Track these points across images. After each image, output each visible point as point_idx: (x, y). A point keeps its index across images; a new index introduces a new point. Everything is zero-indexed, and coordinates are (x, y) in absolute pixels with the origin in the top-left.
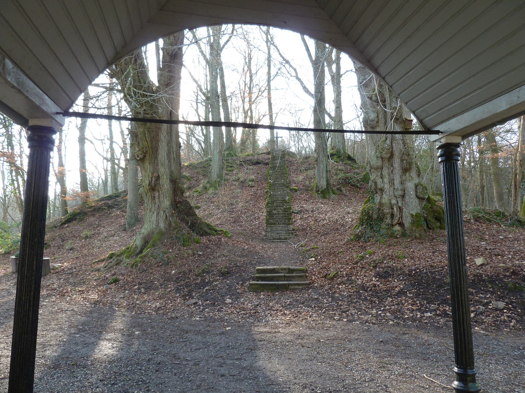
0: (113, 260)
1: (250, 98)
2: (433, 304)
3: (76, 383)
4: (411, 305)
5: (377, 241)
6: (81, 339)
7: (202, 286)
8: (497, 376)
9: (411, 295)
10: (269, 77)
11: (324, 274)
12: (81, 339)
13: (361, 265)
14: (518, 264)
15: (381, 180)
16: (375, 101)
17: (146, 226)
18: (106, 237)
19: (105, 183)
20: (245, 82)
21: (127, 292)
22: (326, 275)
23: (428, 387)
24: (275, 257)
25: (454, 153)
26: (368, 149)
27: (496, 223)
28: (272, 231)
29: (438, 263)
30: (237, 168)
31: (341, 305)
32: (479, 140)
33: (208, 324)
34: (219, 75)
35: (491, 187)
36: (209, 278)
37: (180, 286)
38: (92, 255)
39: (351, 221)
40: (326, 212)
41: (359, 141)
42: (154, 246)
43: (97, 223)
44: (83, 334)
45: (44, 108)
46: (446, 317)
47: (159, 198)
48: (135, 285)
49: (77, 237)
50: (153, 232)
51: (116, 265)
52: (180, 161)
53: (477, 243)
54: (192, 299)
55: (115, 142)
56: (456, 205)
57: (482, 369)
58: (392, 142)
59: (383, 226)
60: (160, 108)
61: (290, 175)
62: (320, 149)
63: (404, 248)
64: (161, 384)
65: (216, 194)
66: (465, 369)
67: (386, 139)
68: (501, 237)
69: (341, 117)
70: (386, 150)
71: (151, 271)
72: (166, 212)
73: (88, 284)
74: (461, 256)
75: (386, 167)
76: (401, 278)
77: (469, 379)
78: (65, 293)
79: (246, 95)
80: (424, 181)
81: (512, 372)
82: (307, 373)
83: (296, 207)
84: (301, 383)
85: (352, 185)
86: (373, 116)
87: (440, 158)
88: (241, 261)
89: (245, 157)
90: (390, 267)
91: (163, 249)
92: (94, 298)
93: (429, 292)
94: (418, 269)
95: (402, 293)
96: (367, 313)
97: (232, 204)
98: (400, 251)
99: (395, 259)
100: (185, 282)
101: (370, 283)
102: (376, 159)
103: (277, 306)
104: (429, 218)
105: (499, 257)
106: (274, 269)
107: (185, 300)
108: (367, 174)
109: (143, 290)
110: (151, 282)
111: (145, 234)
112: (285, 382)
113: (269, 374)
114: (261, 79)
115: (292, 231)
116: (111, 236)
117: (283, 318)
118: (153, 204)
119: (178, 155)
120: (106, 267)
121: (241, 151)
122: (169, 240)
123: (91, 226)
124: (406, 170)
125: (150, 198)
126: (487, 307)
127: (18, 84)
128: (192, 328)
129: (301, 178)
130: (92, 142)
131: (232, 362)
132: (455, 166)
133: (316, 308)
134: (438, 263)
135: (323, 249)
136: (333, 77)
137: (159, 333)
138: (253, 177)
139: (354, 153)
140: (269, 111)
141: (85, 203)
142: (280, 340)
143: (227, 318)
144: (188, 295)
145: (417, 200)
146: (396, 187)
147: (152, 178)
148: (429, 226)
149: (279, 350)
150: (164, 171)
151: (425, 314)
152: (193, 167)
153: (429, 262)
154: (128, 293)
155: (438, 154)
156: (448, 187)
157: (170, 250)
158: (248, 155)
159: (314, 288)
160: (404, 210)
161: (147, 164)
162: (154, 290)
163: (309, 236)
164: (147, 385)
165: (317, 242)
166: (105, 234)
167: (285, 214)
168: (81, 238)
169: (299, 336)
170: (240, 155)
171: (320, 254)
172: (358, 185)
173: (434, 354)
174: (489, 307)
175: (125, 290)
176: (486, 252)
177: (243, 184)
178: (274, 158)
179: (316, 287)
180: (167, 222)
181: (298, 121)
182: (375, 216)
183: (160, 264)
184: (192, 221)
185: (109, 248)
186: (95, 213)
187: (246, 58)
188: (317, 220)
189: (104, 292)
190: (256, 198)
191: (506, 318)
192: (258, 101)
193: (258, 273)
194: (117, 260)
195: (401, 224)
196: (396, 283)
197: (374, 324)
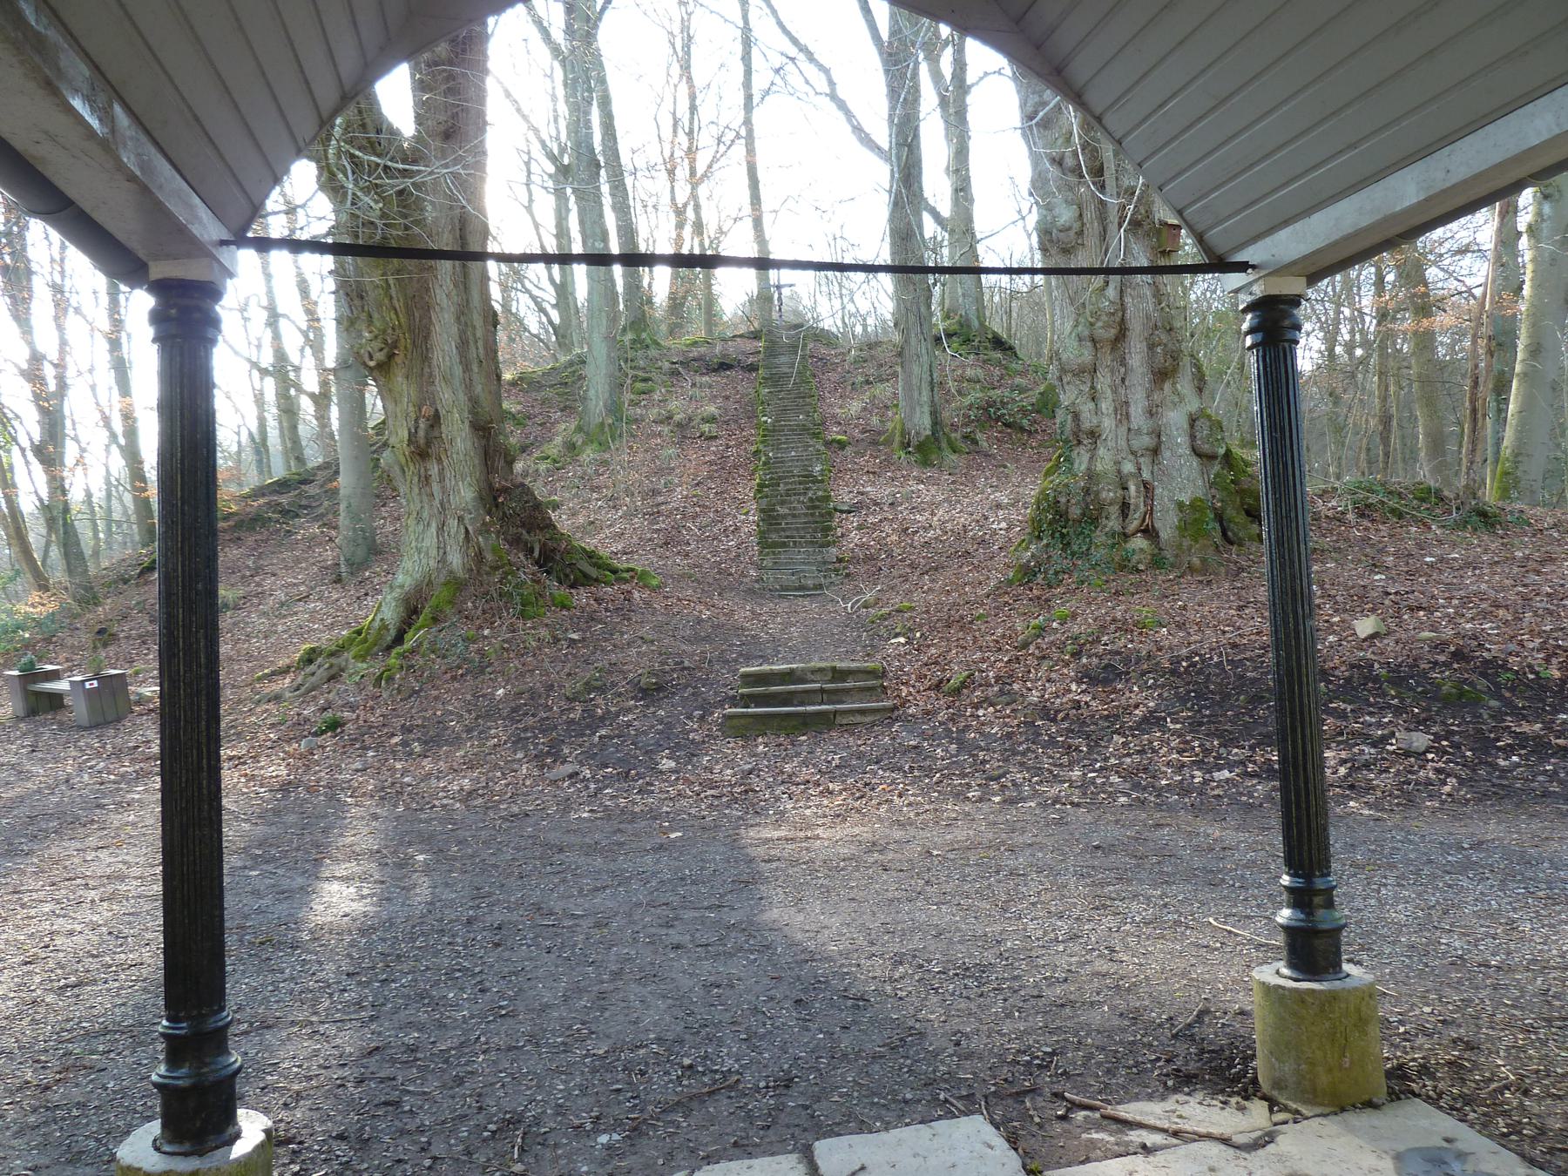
0: (319, 667)
1: (693, 172)
4: (1178, 753)
5: (1083, 582)
6: (267, 881)
7: (588, 726)
8: (1398, 914)
9: (1178, 726)
10: (749, 98)
12: (267, 881)
13: (1037, 652)
14: (1471, 629)
15: (1091, 405)
16: (1073, 171)
17: (407, 564)
18: (282, 604)
20: (674, 114)
21: (371, 754)
22: (941, 681)
23: (1218, 945)
24: (790, 639)
25: (1287, 323)
26: (1053, 316)
27: (1416, 521)
28: (776, 566)
29: (1253, 637)
30: (664, 382)
31: (984, 762)
32: (1380, 282)
33: (616, 826)
34: (603, 172)
35: (1413, 419)
36: (607, 704)
37: (525, 730)
39: (1006, 530)
40: (933, 506)
41: (1025, 289)
42: (435, 620)
43: (250, 563)
44: (270, 867)
45: (195, 230)
46: (1272, 780)
47: (442, 480)
48: (393, 735)
50: (430, 583)
52: (497, 368)
53: (1361, 577)
54: (562, 763)
55: (284, 316)
56: (1290, 462)
57: (1359, 899)
58: (1122, 291)
59: (1099, 537)
60: (429, 208)
61: (821, 398)
62: (912, 318)
63: (1158, 599)
64: (514, 973)
65: (605, 463)
66: (1308, 877)
67: (1107, 283)
68: (1428, 559)
69: (969, 220)
70: (1104, 318)
71: (435, 693)
72: (467, 521)
73: (252, 739)
74: (1302, 593)
76: (1151, 681)
77: (1317, 900)
80: (1218, 406)
81: (1438, 902)
82: (903, 930)
83: (844, 495)
85: (1007, 425)
86: (1066, 215)
90: (1118, 653)
91: (465, 630)
94: (1197, 654)
95: (1152, 721)
96: (1056, 779)
97: (655, 492)
98: (1146, 609)
99: (1132, 631)
101: (1065, 700)
102: (1076, 344)
103: (806, 774)
104: (1230, 512)
105: (1422, 613)
106: (792, 671)
107: (542, 767)
108: (1052, 388)
109: (417, 747)
110: (439, 722)
112: (846, 954)
113: (799, 936)
114: (722, 108)
117: (826, 802)
118: (425, 498)
121: (671, 332)
122: (481, 603)
123: (233, 573)
124: (1162, 375)
125: (416, 479)
126: (1383, 748)
127: (142, 169)
128: (573, 839)
129: (855, 407)
131: (697, 915)
132: (1289, 358)
133: (916, 773)
134: (1253, 637)
135: (927, 612)
136: (944, 103)
137: (484, 856)
138: (712, 409)
139: (1009, 329)
140: (752, 204)
144: (548, 753)
145: (1195, 462)
146: (1134, 426)
147: (416, 421)
148: (1230, 534)
149: (820, 881)
150: (451, 400)
151: (1216, 775)
152: (529, 384)
153: (1228, 635)
155: (1245, 326)
156: (1269, 415)
157: (486, 632)
158: (695, 344)
159: (908, 720)
160: (1158, 491)
161: (400, 379)
162: (451, 744)
163: (886, 577)
164: (478, 979)
167: (812, 515)
169: (874, 844)
171: (921, 626)
172: (1025, 422)
174: (1388, 747)
175: (365, 748)
176: (1387, 602)
178: (772, 351)
182: (1075, 512)
183: (460, 672)
184: (544, 545)
185: (296, 634)
186: (242, 535)
188: (907, 529)
189: (302, 756)
190: (723, 470)
191: (1431, 775)
193: (746, 684)
194: (331, 666)
195: (1149, 532)
196: (1135, 694)
197: (1078, 805)
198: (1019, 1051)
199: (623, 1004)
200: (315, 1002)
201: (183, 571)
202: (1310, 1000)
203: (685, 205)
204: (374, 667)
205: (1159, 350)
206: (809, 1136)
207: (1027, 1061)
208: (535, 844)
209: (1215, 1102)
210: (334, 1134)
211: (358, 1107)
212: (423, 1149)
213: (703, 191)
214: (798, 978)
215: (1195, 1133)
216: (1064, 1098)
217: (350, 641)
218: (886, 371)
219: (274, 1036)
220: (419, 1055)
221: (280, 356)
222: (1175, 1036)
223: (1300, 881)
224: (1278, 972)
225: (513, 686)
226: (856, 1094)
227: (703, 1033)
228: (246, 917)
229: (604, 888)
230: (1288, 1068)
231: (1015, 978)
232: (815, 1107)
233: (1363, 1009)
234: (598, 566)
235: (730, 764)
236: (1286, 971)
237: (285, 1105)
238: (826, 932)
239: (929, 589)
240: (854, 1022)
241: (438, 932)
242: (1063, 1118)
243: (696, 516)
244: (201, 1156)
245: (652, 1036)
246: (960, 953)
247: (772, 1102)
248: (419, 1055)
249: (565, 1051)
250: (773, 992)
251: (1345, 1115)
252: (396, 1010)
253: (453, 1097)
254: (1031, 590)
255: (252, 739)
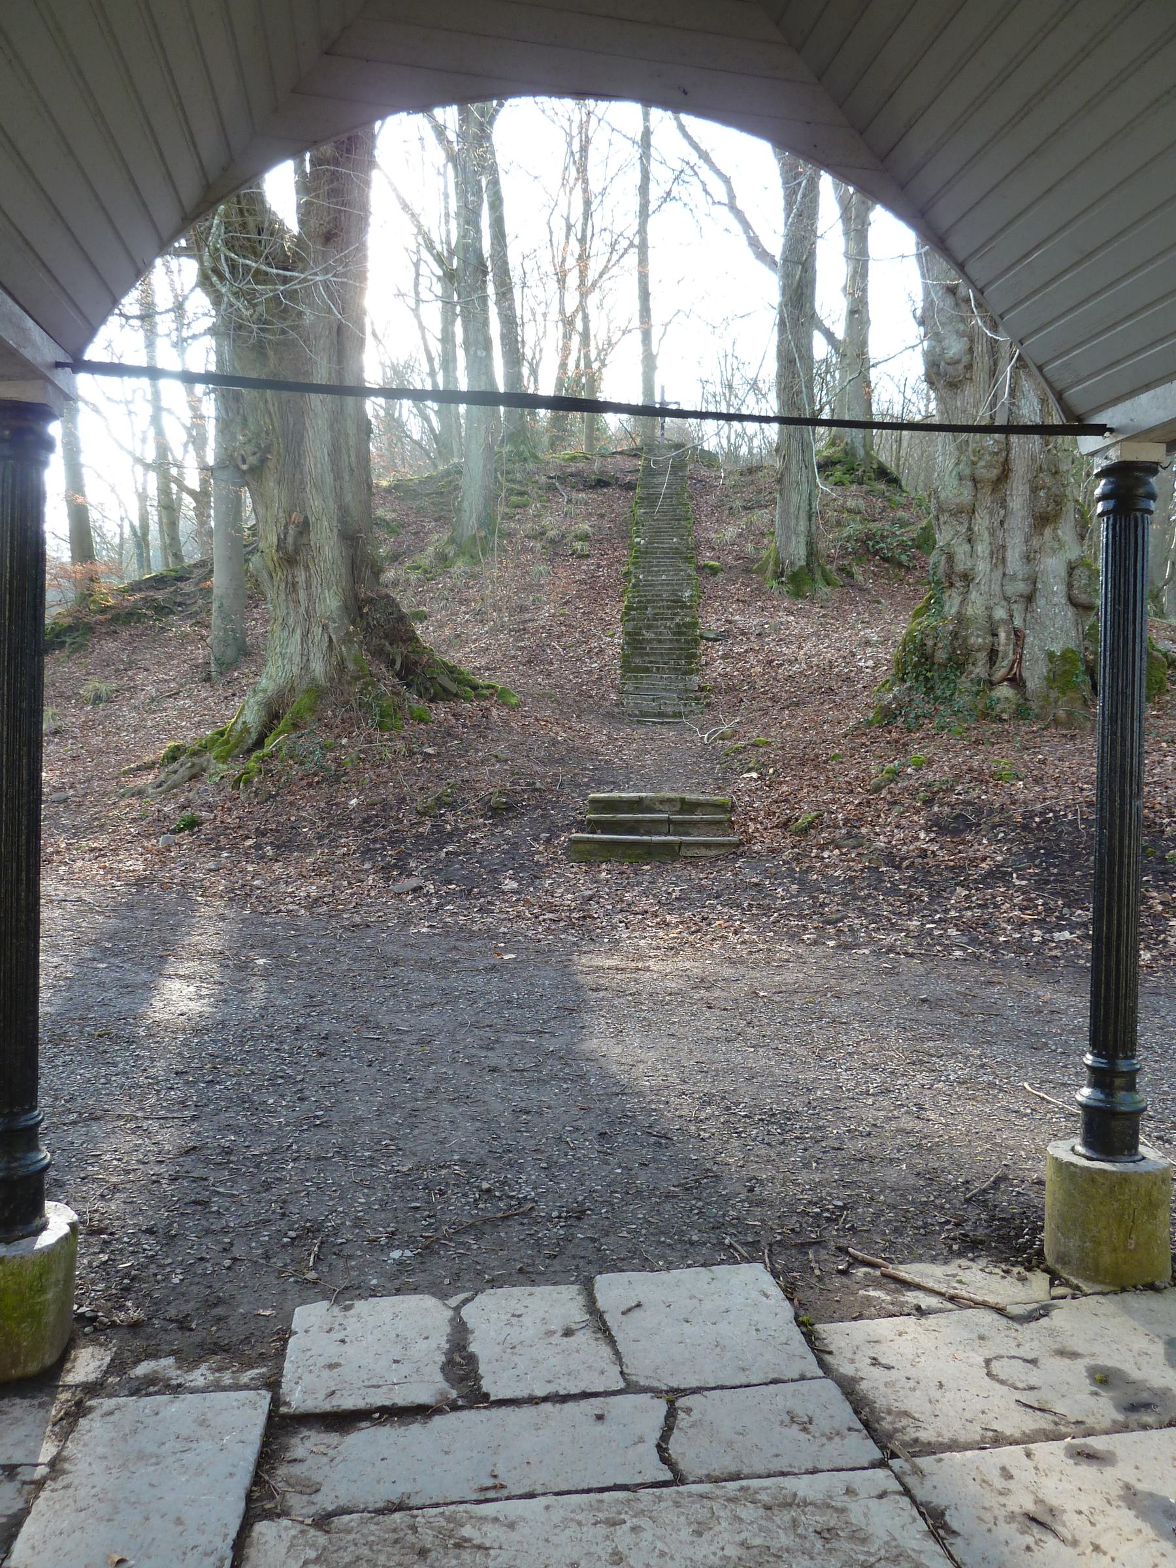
2: (1081, 909)
3: (114, 1078)
4: (1020, 910)
5: (943, 728)
7: (436, 841)
9: (1024, 883)
11: (783, 818)
12: (113, 974)
13: (889, 796)
15: (967, 547)
17: (270, 669)
18: (153, 700)
19: (141, 539)
20: (567, 219)
21: (225, 854)
22: (789, 820)
23: (1029, 1111)
24: (644, 766)
25: (1141, 491)
28: (637, 691)
31: (823, 905)
33: (452, 944)
34: (490, 277)
36: (456, 821)
37: (375, 841)
38: (118, 751)
40: (802, 639)
42: (295, 726)
43: (125, 657)
44: (116, 961)
45: (28, 353)
47: (308, 587)
48: (247, 837)
49: (69, 698)
50: (292, 689)
51: (190, 779)
52: (369, 476)
55: (168, 410)
56: (1131, 636)
59: (964, 683)
61: (697, 522)
62: (794, 444)
63: (1019, 751)
64: (335, 1085)
65: (473, 576)
69: (864, 344)
72: (331, 630)
73: (114, 832)
75: (986, 508)
77: (1118, 1082)
78: (52, 854)
79: (571, 262)
82: (717, 1070)
83: (711, 623)
84: (698, 1092)
85: (885, 559)
87: (1100, 503)
88: (545, 776)
89: (563, 463)
90: (970, 803)
91: (324, 738)
92: (134, 871)
93: (1073, 875)
94: (1051, 811)
95: (997, 875)
97: (523, 609)
99: (987, 782)
100: (387, 831)
101: (911, 848)
102: (956, 482)
103: (645, 903)
106: (641, 800)
107: (388, 879)
109: (269, 851)
110: (292, 828)
111: (269, 694)
113: (614, 1068)
115: (698, 694)
116: (170, 696)
117: (661, 934)
118: (291, 605)
119: (364, 459)
120: (160, 786)
121: (552, 445)
122: (340, 712)
123: (108, 665)
124: (1043, 520)
128: (409, 953)
130: (96, 409)
131: (518, 1039)
132: (1140, 529)
135: (783, 748)
137: (322, 965)
138: (586, 527)
140: (642, 316)
141: (86, 596)
142: (649, 989)
143: (506, 930)
144: (395, 865)
145: (1070, 612)
146: (1010, 571)
147: (286, 527)
149: (643, 1014)
151: (1056, 935)
153: (1086, 793)
154: (227, 857)
155: (1098, 492)
156: (1114, 587)
157: (344, 741)
158: (573, 459)
159: (752, 856)
160: (1029, 640)
161: (272, 484)
162: (302, 850)
163: (746, 708)
164: (299, 1087)
165: (769, 726)
166: (152, 690)
167: (677, 641)
168: (82, 702)
169: (702, 981)
170: (547, 456)
171: (775, 762)
172: (904, 558)
173: (1061, 1035)
175: (220, 849)
177: (556, 548)
179: (757, 853)
180: (334, 659)
181: (729, 352)
182: (941, 656)
183: (316, 779)
185: (164, 730)
186: (118, 629)
187: (572, 138)
188: (772, 661)
189: (159, 853)
190: (593, 590)
192: (605, 283)
193: (595, 810)
194: (193, 765)
195: (1016, 681)
196: (984, 846)
197: (912, 955)
198: (810, 1202)
199: (433, 1124)
200: (143, 1098)
201: (9, 691)
202: (1100, 1180)
203: (574, 316)
204: (232, 769)
205: (1042, 493)
206: (593, 1269)
207: (817, 1214)
208: (371, 956)
209: (996, 1270)
210: (144, 1228)
211: (169, 1204)
212: (225, 1250)
213: (592, 300)
214: (607, 1110)
215: (971, 1300)
216: (848, 1253)
217: (213, 741)
218: (764, 497)
219: (100, 1128)
220: (232, 1158)
221: (163, 449)
222: (968, 1201)
223: (1102, 1063)
224: (1073, 1149)
225: (367, 797)
226: (644, 1231)
227: (506, 1158)
228: (89, 1008)
229: (432, 1005)
230: (1074, 1243)
231: (819, 1128)
232: (602, 1240)
233: (1155, 1193)
234: (459, 682)
235: (572, 889)
236: (1080, 1149)
237: (102, 1196)
238: (641, 1066)
239: (788, 725)
240: (654, 1160)
241: (267, 1037)
242: (844, 1273)
243: (562, 635)
244: (8, 1243)
245: (456, 1157)
246: (769, 1099)
247: (561, 1232)
248: (232, 1158)
249: (371, 1166)
250: (579, 1123)
251: (1125, 1295)
252: (217, 1112)
253: (259, 1202)
254: (890, 732)
255: (114, 832)
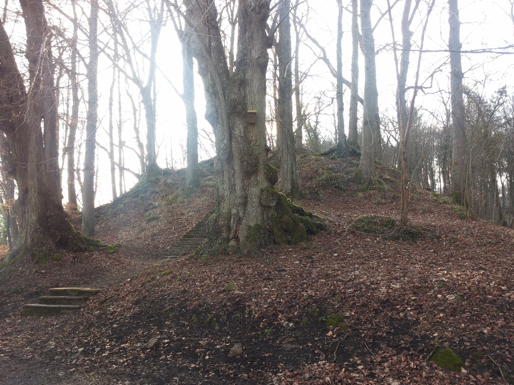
62: (284, 146)
195: (236, 238)
205: (245, 163)
